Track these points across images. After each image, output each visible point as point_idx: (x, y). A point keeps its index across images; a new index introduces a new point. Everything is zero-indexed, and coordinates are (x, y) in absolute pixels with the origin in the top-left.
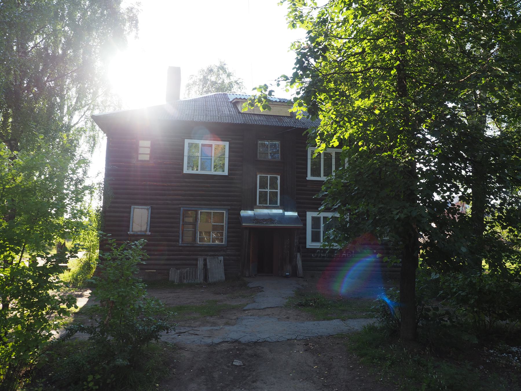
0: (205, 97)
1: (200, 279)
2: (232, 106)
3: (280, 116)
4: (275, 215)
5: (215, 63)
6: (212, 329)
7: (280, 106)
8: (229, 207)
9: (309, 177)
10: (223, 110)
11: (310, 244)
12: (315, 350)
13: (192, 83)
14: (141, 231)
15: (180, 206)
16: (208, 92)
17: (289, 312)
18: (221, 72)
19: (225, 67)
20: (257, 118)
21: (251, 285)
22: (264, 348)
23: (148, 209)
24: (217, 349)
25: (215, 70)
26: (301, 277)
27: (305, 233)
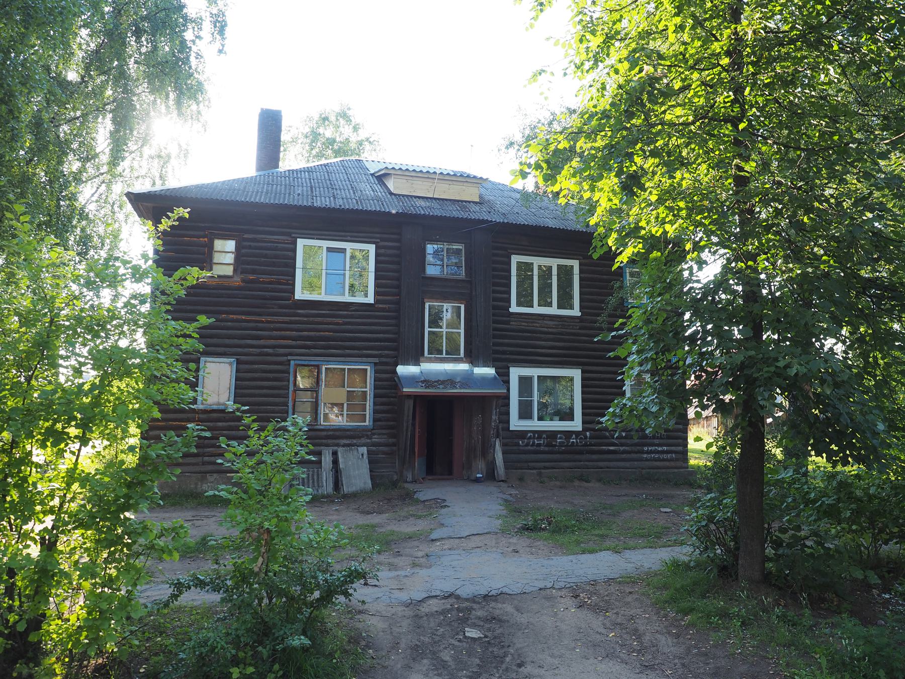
0: (325, 165)
1: (328, 487)
2: (377, 182)
3: (462, 201)
4: (456, 373)
5: (332, 107)
6: (398, 576)
7: (462, 184)
8: (376, 360)
9: (514, 308)
10: (362, 189)
11: (516, 423)
12: (595, 606)
13: (291, 140)
14: (219, 404)
15: (289, 358)
16: (322, 157)
17: (511, 540)
18: (342, 121)
19: (349, 113)
20: (423, 203)
21: (422, 496)
22: (504, 605)
23: (230, 364)
24: (423, 610)
25: (332, 118)
26: (502, 481)
27: (508, 405)
